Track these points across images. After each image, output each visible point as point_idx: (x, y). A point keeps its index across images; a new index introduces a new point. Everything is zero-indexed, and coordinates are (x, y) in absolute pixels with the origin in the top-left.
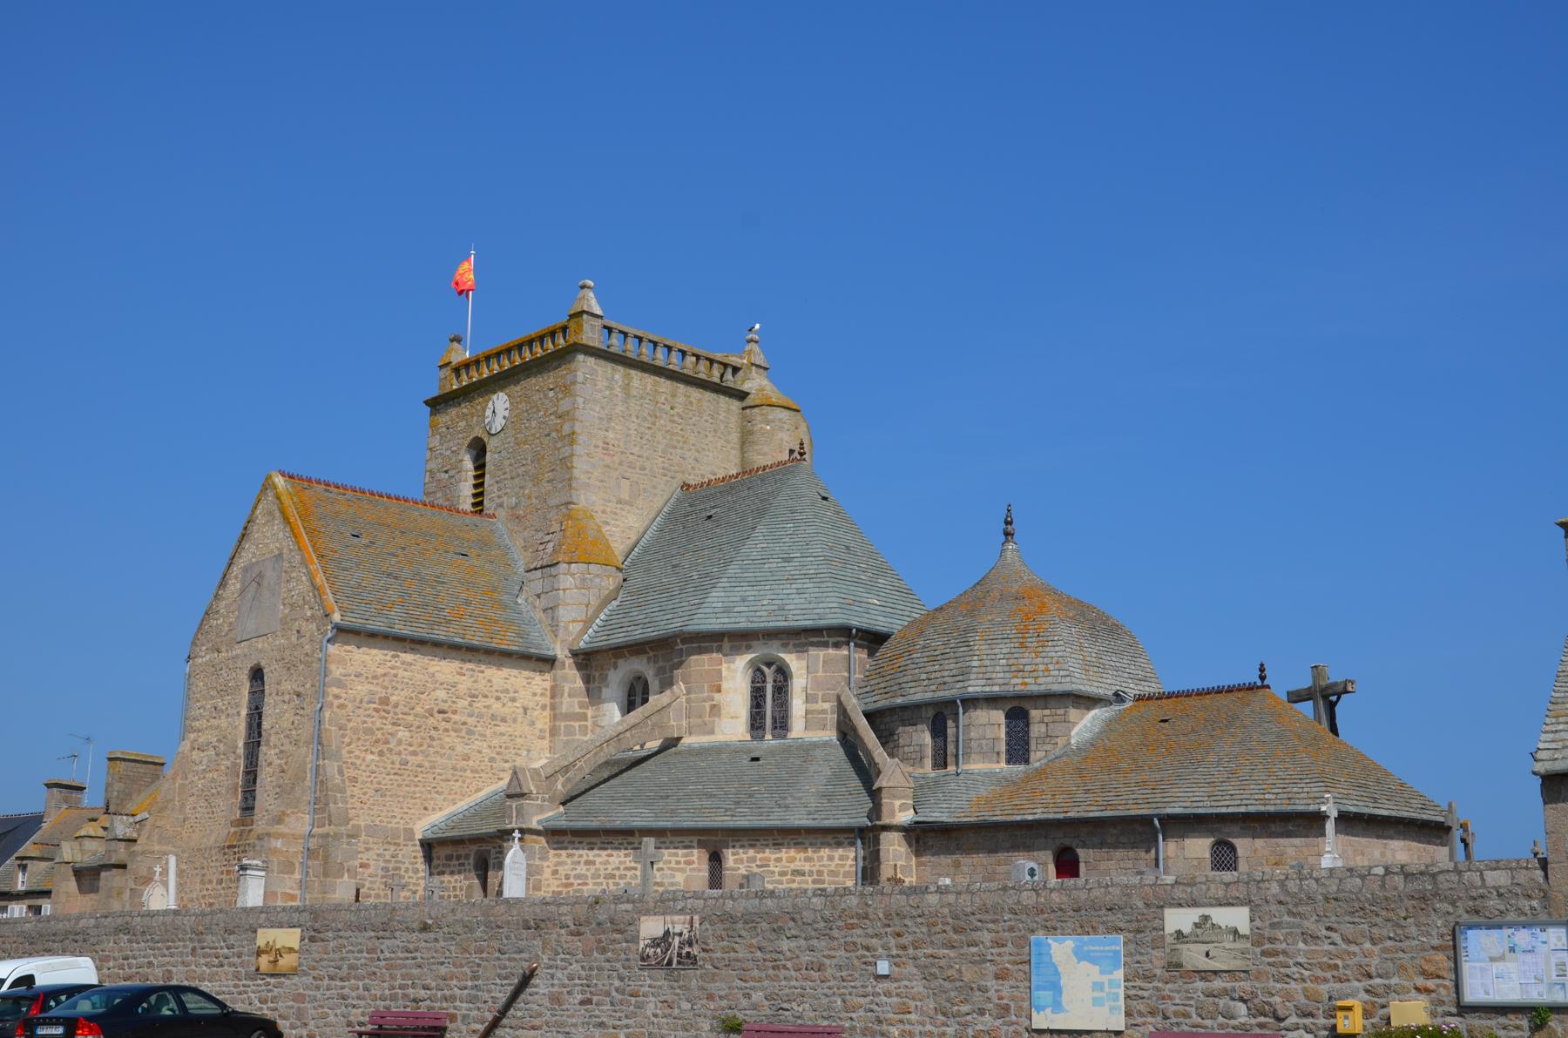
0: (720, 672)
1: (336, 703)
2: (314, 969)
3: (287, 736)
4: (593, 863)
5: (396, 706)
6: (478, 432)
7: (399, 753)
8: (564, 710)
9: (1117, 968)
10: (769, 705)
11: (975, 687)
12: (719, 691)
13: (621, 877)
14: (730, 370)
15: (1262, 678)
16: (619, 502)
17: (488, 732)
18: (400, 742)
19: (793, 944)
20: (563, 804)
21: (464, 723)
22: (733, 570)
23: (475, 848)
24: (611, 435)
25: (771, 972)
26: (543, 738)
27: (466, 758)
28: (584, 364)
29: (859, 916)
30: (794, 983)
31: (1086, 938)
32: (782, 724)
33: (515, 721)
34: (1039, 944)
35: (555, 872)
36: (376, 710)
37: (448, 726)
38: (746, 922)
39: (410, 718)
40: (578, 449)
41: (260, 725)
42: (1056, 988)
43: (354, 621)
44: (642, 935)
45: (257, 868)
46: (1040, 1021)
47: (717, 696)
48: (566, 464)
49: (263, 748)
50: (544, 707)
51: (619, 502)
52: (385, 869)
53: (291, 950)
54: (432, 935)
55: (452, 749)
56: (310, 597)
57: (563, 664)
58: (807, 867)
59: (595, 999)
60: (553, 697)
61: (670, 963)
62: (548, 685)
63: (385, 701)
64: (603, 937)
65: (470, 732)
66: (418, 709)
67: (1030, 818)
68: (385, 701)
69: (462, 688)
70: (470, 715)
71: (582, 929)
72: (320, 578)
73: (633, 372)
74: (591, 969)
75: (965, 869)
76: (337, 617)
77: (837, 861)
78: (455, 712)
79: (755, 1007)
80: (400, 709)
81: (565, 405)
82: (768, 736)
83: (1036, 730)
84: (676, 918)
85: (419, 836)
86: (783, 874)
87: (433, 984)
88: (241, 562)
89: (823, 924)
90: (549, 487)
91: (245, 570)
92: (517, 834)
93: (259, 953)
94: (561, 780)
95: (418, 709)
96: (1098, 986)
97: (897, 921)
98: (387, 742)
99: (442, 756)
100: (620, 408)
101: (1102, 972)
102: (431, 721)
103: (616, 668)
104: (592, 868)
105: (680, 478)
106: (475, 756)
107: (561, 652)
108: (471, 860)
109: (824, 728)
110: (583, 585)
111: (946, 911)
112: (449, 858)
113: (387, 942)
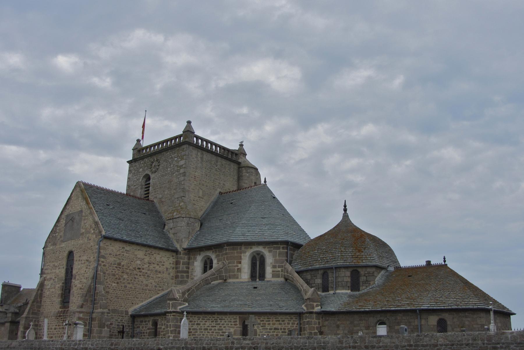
0: (241, 256)
1: (102, 264)
3: (83, 276)
4: (200, 324)
7: (124, 283)
8: (180, 269)
11: (340, 263)
12: (240, 263)
13: (211, 330)
14: (230, 153)
15: (445, 261)
17: (154, 277)
18: (124, 279)
21: (146, 273)
23: (152, 318)
24: (196, 174)
26: (173, 279)
27: (147, 285)
32: (262, 276)
33: (163, 273)
36: (116, 267)
37: (141, 274)
39: (128, 271)
41: (72, 272)
45: (80, 324)
47: (239, 265)
49: (73, 280)
50: (173, 268)
51: (199, 197)
55: (142, 282)
57: (180, 253)
58: (280, 327)
60: (176, 265)
62: (174, 260)
63: (119, 264)
65: (148, 276)
67: (368, 310)
68: (119, 264)
70: (148, 270)
72: (97, 219)
73: (204, 152)
75: (341, 328)
76: (103, 233)
77: (291, 325)
78: (143, 269)
82: (258, 280)
83: (362, 279)
85: (130, 313)
88: (66, 213)
90: (175, 191)
92: (185, 313)
94: (187, 294)
95: (131, 268)
98: (120, 279)
99: (139, 284)
100: (200, 165)
102: (135, 272)
103: (200, 255)
104: (199, 326)
105: (219, 190)
106: (150, 285)
108: (151, 323)
109: (279, 277)
112: (142, 322)
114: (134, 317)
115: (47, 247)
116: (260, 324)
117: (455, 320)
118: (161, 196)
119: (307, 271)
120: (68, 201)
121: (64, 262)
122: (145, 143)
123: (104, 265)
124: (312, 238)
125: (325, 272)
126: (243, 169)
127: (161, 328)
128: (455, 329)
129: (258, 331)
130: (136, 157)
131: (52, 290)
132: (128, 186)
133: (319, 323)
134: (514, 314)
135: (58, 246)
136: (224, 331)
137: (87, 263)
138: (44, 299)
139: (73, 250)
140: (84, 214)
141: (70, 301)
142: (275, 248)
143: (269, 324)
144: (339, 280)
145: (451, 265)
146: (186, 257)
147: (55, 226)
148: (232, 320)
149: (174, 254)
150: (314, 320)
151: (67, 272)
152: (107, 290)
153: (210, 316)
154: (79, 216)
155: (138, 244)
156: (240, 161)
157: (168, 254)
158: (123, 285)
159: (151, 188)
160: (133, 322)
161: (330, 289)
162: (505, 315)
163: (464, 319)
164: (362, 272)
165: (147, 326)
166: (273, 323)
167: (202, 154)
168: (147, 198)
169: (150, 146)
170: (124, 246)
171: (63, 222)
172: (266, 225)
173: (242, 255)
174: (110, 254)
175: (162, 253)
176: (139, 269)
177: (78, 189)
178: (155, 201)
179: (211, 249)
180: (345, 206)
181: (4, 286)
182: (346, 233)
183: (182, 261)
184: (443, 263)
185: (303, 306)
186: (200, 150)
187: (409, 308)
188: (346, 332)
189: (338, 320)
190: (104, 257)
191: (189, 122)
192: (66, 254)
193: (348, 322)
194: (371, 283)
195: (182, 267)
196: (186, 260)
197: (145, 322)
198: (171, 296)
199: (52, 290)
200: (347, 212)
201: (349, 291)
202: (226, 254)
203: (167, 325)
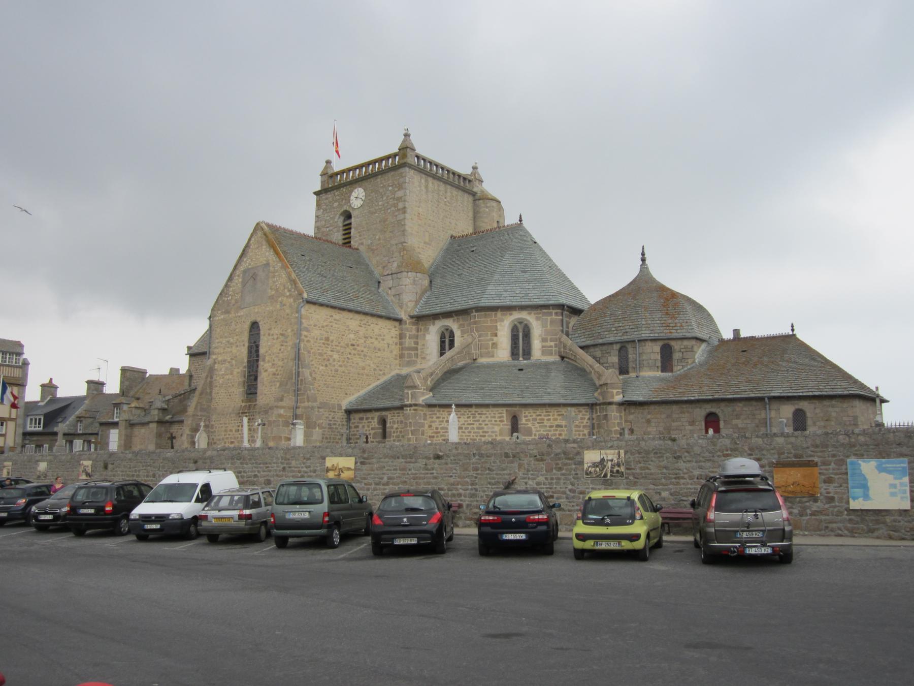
1: (306, 339)
2: (365, 479)
5: (332, 341)
6: (346, 208)
8: (407, 345)
9: (905, 476)
10: (521, 340)
11: (645, 334)
15: (793, 330)
16: (425, 243)
18: (334, 360)
19: (688, 465)
20: (431, 390)
22: (496, 277)
23: (378, 414)
24: (421, 210)
25: (674, 480)
27: (364, 369)
28: (409, 174)
29: (732, 450)
30: (689, 486)
31: (883, 460)
32: (527, 354)
34: (852, 463)
35: (430, 426)
37: (356, 352)
38: (656, 453)
40: (407, 215)
41: (257, 351)
42: (865, 487)
43: (313, 297)
44: (586, 460)
45: (300, 424)
46: (854, 505)
47: (495, 338)
48: (401, 224)
49: (261, 363)
52: (330, 425)
53: (349, 469)
54: (443, 461)
56: (289, 285)
58: (564, 423)
59: (555, 495)
61: (605, 476)
62: (397, 333)
64: (559, 462)
66: (342, 344)
68: (327, 339)
69: (361, 333)
71: (545, 457)
72: (293, 275)
74: (552, 479)
75: (653, 424)
76: (305, 296)
79: (664, 499)
80: (335, 343)
81: (400, 194)
82: (521, 359)
83: (676, 356)
84: (608, 451)
85: (344, 408)
86: (551, 427)
87: (446, 487)
88: (242, 268)
89: (707, 454)
91: (245, 272)
92: (453, 406)
93: (328, 470)
95: (342, 344)
96: (893, 486)
97: (757, 452)
101: (895, 478)
102: (348, 350)
103: (434, 324)
107: (403, 316)
108: (376, 420)
109: (551, 354)
110: (414, 283)
111: (790, 446)
112: (362, 419)
113: (412, 465)
114: (349, 412)
115: (215, 316)
116: (535, 420)
117: (818, 411)
118: (369, 242)
119: (595, 346)
120: (244, 251)
121: (245, 337)
122: (337, 167)
123: (308, 341)
124: (593, 302)
125: (623, 347)
126: (481, 201)
127: (392, 427)
128: (818, 423)
129: (534, 429)
130: (326, 186)
131: (227, 377)
132: (317, 228)
133: (621, 417)
134: (51, 379)
135: (232, 315)
136: (485, 430)
137: (282, 338)
138: (215, 390)
139: (258, 320)
140: (271, 269)
141: (259, 391)
142: (544, 314)
143: (549, 420)
144: (644, 357)
145: (801, 335)
146: (414, 327)
147: (226, 286)
148: (497, 415)
149: (397, 324)
150: (614, 413)
151: (250, 352)
152: (314, 375)
153: (465, 409)
154: (263, 271)
155: (350, 311)
156: (475, 190)
157: (389, 324)
158: (333, 369)
159: (353, 231)
160: (349, 420)
161: (630, 370)
162: (872, 399)
163: (830, 409)
164: (676, 345)
165: (369, 425)
166: (553, 418)
167: (426, 181)
168: (347, 242)
169: (342, 172)
170: (333, 314)
171: (238, 280)
172: (529, 281)
173: (498, 324)
174: (315, 325)
175: (382, 323)
176: (353, 345)
177: (260, 233)
178: (362, 248)
179: (452, 316)
180: (643, 254)
181: (124, 370)
182: (644, 292)
183: (408, 334)
184: (791, 333)
185: (596, 394)
186: (424, 176)
187: (753, 395)
188: (661, 429)
189: (649, 413)
190: (307, 330)
191: (407, 135)
192: (247, 326)
193: (663, 416)
194: (690, 361)
195: (408, 342)
196: (414, 332)
197: (367, 419)
198: (409, 383)
199: (227, 377)
200: (647, 262)
201: (659, 374)
202: (475, 323)
203: (406, 424)
